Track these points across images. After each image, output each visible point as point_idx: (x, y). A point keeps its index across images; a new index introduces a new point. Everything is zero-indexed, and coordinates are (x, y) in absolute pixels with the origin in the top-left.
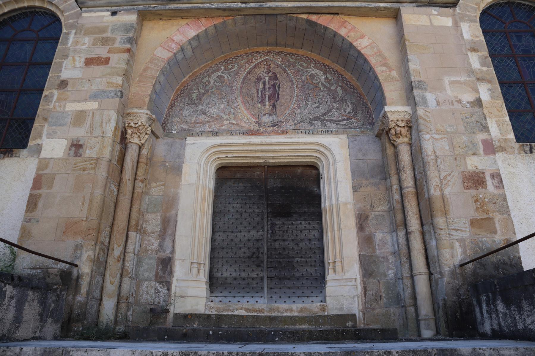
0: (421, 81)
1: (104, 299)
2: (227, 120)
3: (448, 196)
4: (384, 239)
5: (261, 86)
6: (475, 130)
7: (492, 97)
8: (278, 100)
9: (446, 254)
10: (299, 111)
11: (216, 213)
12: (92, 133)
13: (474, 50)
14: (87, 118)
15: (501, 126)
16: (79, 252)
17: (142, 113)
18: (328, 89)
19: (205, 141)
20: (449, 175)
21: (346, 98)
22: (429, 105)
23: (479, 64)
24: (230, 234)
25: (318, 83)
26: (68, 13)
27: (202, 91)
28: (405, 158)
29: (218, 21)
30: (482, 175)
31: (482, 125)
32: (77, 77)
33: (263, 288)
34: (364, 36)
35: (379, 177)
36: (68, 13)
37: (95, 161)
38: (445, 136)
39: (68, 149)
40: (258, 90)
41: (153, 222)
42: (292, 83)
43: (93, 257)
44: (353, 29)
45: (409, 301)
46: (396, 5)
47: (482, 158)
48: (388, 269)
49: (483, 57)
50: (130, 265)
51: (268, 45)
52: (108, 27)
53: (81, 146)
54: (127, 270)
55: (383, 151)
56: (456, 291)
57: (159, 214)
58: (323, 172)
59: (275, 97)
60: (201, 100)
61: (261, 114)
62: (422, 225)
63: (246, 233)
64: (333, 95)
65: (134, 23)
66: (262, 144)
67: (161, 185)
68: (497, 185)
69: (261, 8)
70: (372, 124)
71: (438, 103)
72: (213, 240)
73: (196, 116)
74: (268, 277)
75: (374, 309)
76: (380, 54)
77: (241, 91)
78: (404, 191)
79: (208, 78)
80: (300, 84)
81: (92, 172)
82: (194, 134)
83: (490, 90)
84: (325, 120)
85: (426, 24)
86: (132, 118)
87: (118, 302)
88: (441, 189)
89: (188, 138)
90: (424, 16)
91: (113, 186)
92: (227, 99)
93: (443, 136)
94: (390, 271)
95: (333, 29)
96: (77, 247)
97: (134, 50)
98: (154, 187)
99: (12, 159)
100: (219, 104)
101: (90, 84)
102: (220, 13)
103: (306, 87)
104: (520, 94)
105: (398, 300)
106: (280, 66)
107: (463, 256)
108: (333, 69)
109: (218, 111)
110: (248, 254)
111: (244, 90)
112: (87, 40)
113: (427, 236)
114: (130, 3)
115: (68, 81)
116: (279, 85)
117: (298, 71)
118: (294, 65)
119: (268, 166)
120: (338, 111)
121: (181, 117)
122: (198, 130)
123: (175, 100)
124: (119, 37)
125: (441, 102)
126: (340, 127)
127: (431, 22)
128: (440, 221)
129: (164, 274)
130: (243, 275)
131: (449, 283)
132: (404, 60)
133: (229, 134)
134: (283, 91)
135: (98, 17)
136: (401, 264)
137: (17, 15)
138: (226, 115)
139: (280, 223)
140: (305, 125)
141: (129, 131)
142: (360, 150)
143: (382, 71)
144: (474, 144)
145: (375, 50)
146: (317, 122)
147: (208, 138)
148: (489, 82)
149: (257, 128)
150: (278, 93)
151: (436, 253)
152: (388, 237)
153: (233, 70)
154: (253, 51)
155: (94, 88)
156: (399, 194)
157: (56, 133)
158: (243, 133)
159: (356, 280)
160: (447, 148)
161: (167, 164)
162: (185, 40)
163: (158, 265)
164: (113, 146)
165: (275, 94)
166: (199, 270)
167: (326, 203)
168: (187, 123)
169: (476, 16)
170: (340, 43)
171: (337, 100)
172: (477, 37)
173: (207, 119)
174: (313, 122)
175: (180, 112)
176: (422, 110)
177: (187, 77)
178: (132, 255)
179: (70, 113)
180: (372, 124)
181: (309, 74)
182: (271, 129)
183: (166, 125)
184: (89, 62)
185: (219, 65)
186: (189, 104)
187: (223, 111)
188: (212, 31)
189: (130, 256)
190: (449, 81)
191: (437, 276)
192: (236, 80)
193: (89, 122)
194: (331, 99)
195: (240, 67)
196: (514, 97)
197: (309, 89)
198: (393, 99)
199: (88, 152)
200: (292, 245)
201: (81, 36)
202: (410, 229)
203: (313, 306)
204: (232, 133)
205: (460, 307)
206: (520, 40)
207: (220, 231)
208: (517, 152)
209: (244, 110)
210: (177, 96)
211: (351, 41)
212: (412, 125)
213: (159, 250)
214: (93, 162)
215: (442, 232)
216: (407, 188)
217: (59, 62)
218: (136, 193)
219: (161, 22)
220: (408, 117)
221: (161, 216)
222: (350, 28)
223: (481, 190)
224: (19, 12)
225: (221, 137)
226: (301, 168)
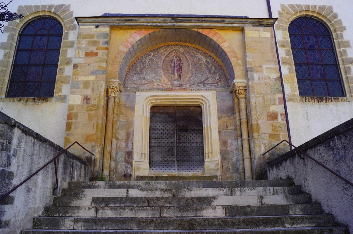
0: (252, 68)
1: (104, 170)
2: (156, 83)
3: (260, 124)
4: (232, 143)
5: (173, 65)
6: (275, 93)
7: (289, 73)
8: (182, 72)
9: (257, 149)
10: (192, 78)
11: (151, 129)
12: (93, 92)
13: (283, 46)
15: (292, 88)
16: (94, 149)
17: (116, 81)
18: (207, 67)
20: (261, 114)
21: (216, 71)
22: (255, 80)
23: (285, 54)
24: (158, 140)
25: (202, 63)
26: (66, 21)
27: (142, 67)
28: (243, 105)
29: (151, 31)
30: (276, 114)
31: (279, 90)
32: (81, 62)
33: (174, 165)
34: (226, 41)
35: (231, 113)
36: (66, 21)
37: (96, 106)
38: (261, 95)
39: (83, 100)
41: (122, 134)
45: (241, 171)
46: (242, 25)
47: (277, 106)
48: (233, 156)
49: (288, 50)
50: (114, 155)
51: (176, 41)
52: (94, 34)
54: (112, 157)
55: (233, 100)
56: (260, 166)
57: (125, 131)
58: (204, 110)
59: (180, 70)
60: (142, 72)
61: (173, 80)
62: (249, 137)
63: (166, 140)
64: (209, 70)
65: (108, 32)
66: (174, 96)
68: (283, 119)
69: (173, 26)
70: (229, 86)
71: (259, 79)
72: (150, 143)
73: (140, 80)
74: (177, 160)
75: (226, 174)
76: (234, 52)
77: (163, 67)
78: (241, 120)
81: (96, 112)
83: (289, 69)
84: (205, 83)
85: (257, 36)
86: (111, 84)
87: (110, 172)
88: (257, 121)
89: (137, 92)
90: (256, 31)
92: (155, 71)
93: (260, 95)
94: (234, 158)
95: (210, 37)
96: (93, 147)
97: (109, 48)
98: (121, 117)
99: (47, 103)
101: (89, 66)
102: (153, 27)
103: (196, 65)
104: (305, 70)
105: (237, 170)
106: (182, 53)
107: (264, 151)
108: (210, 55)
109: (151, 78)
110: (167, 150)
111: (164, 67)
112: (84, 42)
113: (250, 142)
114: (105, 21)
115: (77, 65)
116: (182, 64)
117: (192, 56)
118: (189, 53)
119: (177, 106)
121: (132, 81)
122: (142, 88)
123: (128, 71)
124: (101, 40)
125: (261, 78)
126: (212, 87)
127: (259, 35)
128: (255, 134)
129: (129, 159)
130: (166, 159)
131: (257, 162)
132: (245, 56)
134: (184, 67)
135: (88, 28)
136: (239, 154)
137: (35, 20)
138: (155, 80)
139: (183, 134)
140: (195, 86)
141: (110, 90)
142: (222, 99)
143: (234, 61)
144: (274, 100)
145: (231, 49)
147: (147, 92)
148: (289, 64)
149: (171, 87)
151: (253, 149)
152: (234, 142)
154: (168, 44)
155: (92, 69)
156: (239, 122)
157: (75, 92)
158: (164, 90)
159: (218, 161)
160: (261, 101)
161: (127, 106)
162: (134, 42)
163: (126, 155)
164: (104, 99)
165: (180, 69)
166: (145, 157)
167: (205, 125)
169: (286, 27)
170: (214, 44)
171: (211, 73)
172: (286, 39)
173: (146, 82)
175: (132, 78)
176: (251, 82)
177: (134, 58)
178: (114, 150)
179: (81, 82)
180: (229, 86)
182: (178, 88)
183: (125, 85)
184: (87, 54)
185: (150, 52)
186: (136, 74)
187: (154, 78)
188: (148, 36)
189: (113, 151)
190: (266, 67)
191: (253, 159)
195: (162, 53)
196: (302, 72)
197: (198, 66)
198: (238, 75)
199: (93, 101)
200: (189, 145)
201: (81, 39)
202: (243, 138)
203: (199, 173)
204: (159, 90)
205: (262, 172)
206: (309, 40)
207: (153, 138)
208: (298, 101)
209: (164, 78)
210: (129, 69)
211: (219, 44)
212: (246, 89)
213: (126, 148)
214: (96, 107)
215: (256, 140)
216: (243, 119)
217: (65, 50)
219: (121, 31)
220: (245, 85)
221: (126, 131)
223: (275, 121)
224: (37, 18)
225: (154, 92)
226: (193, 107)
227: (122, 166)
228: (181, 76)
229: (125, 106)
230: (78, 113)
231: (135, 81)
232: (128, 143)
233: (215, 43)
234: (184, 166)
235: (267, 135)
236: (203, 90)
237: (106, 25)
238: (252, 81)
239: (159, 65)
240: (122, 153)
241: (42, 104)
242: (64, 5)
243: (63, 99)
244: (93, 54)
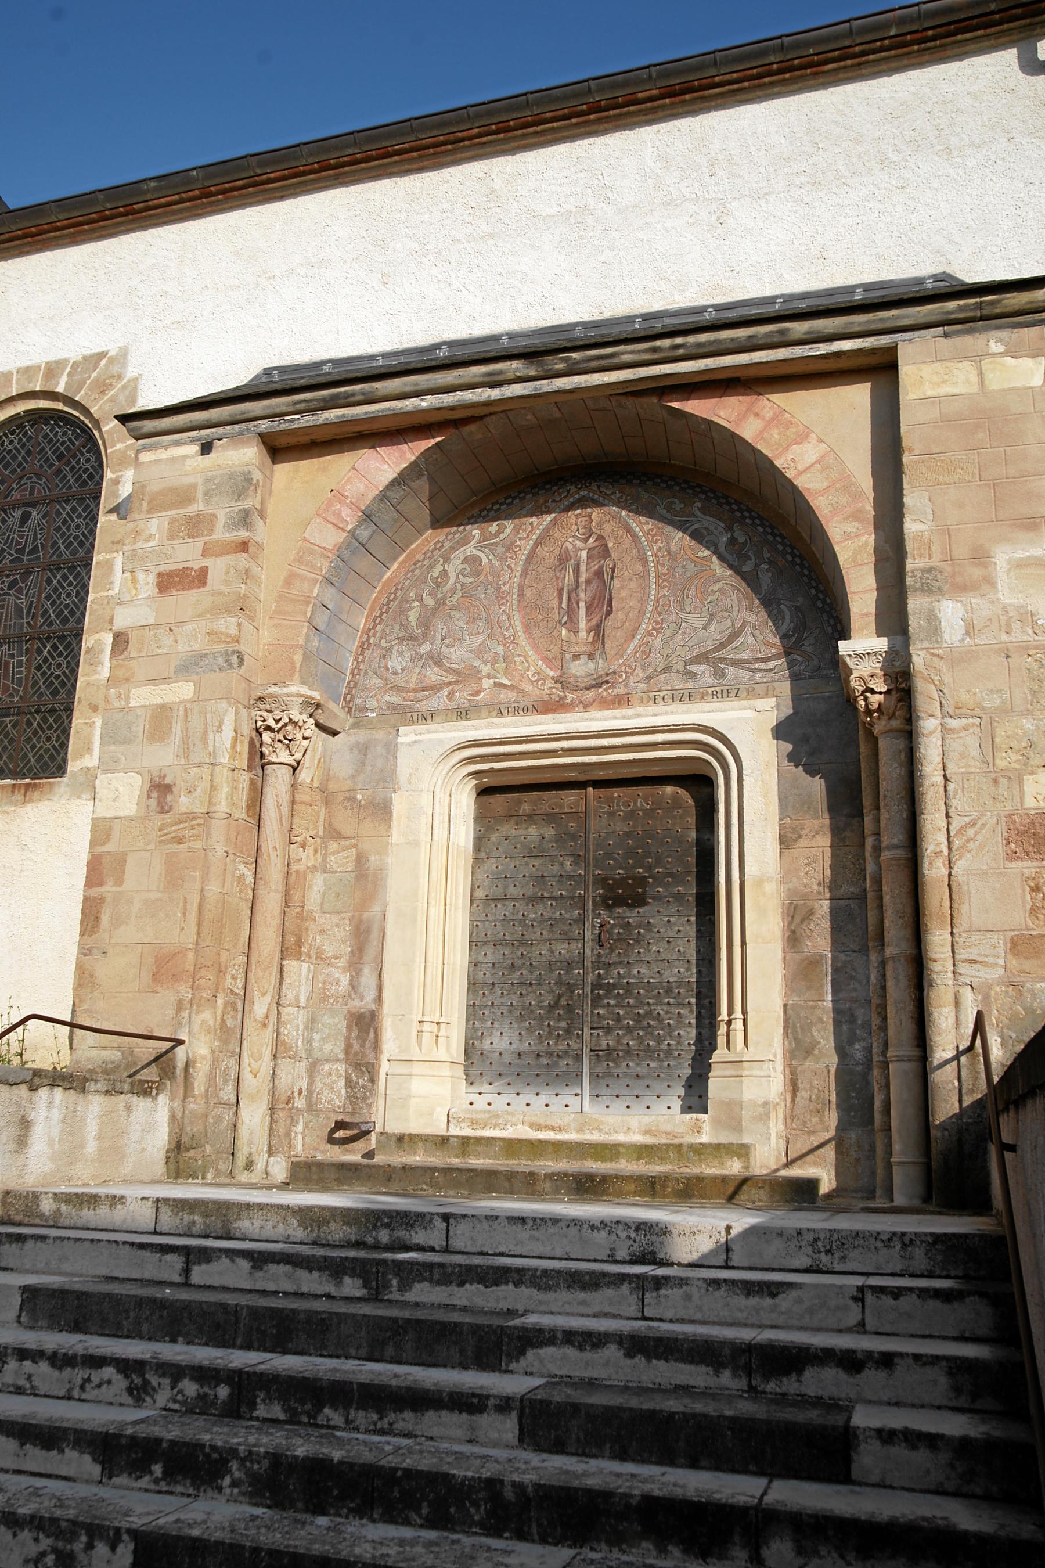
0: (930, 570)
2: (489, 677)
5: (569, 577)
8: (609, 613)
10: (659, 640)
12: (187, 757)
14: (174, 723)
19: (441, 735)
20: (972, 824)
22: (946, 636)
27: (430, 602)
42: (644, 561)
43: (211, 1023)
44: (778, 418)
52: (194, 486)
54: (284, 1043)
59: (603, 604)
61: (568, 656)
67: (348, 848)
77: (521, 595)
80: (663, 565)
82: (415, 718)
84: (722, 660)
89: (402, 729)
91: (242, 867)
92: (488, 620)
94: (857, 1046)
98: (333, 854)
100: (470, 634)
103: (679, 570)
108: (750, 511)
111: (528, 593)
116: (613, 571)
120: (757, 633)
124: (223, 511)
129: (363, 1046)
133: (495, 713)
134: (622, 587)
135: (173, 460)
138: (485, 662)
143: (847, 537)
146: (703, 667)
150: (610, 595)
153: (502, 536)
155: (181, 647)
158: (525, 710)
163: (349, 1028)
168: (396, 688)
174: (694, 668)
182: (589, 695)
183: (353, 697)
184: (167, 582)
186: (401, 640)
187: (479, 653)
190: (1009, 561)
192: (509, 567)
193: (179, 732)
194: (739, 602)
199: (183, 799)
201: (142, 516)
210: (374, 620)
217: (107, 561)
218: (294, 874)
222: (768, 415)
227: (334, 1082)
229: (349, 799)
230: (125, 854)
231: (396, 673)
232: (359, 973)
234: (624, 1082)
235: (1000, 941)
236: (709, 698)
237: (241, 433)
238: (926, 645)
239: (503, 588)
240: (337, 1020)
241: (21, 811)
242: (102, 355)
243: (89, 786)
244: (188, 576)
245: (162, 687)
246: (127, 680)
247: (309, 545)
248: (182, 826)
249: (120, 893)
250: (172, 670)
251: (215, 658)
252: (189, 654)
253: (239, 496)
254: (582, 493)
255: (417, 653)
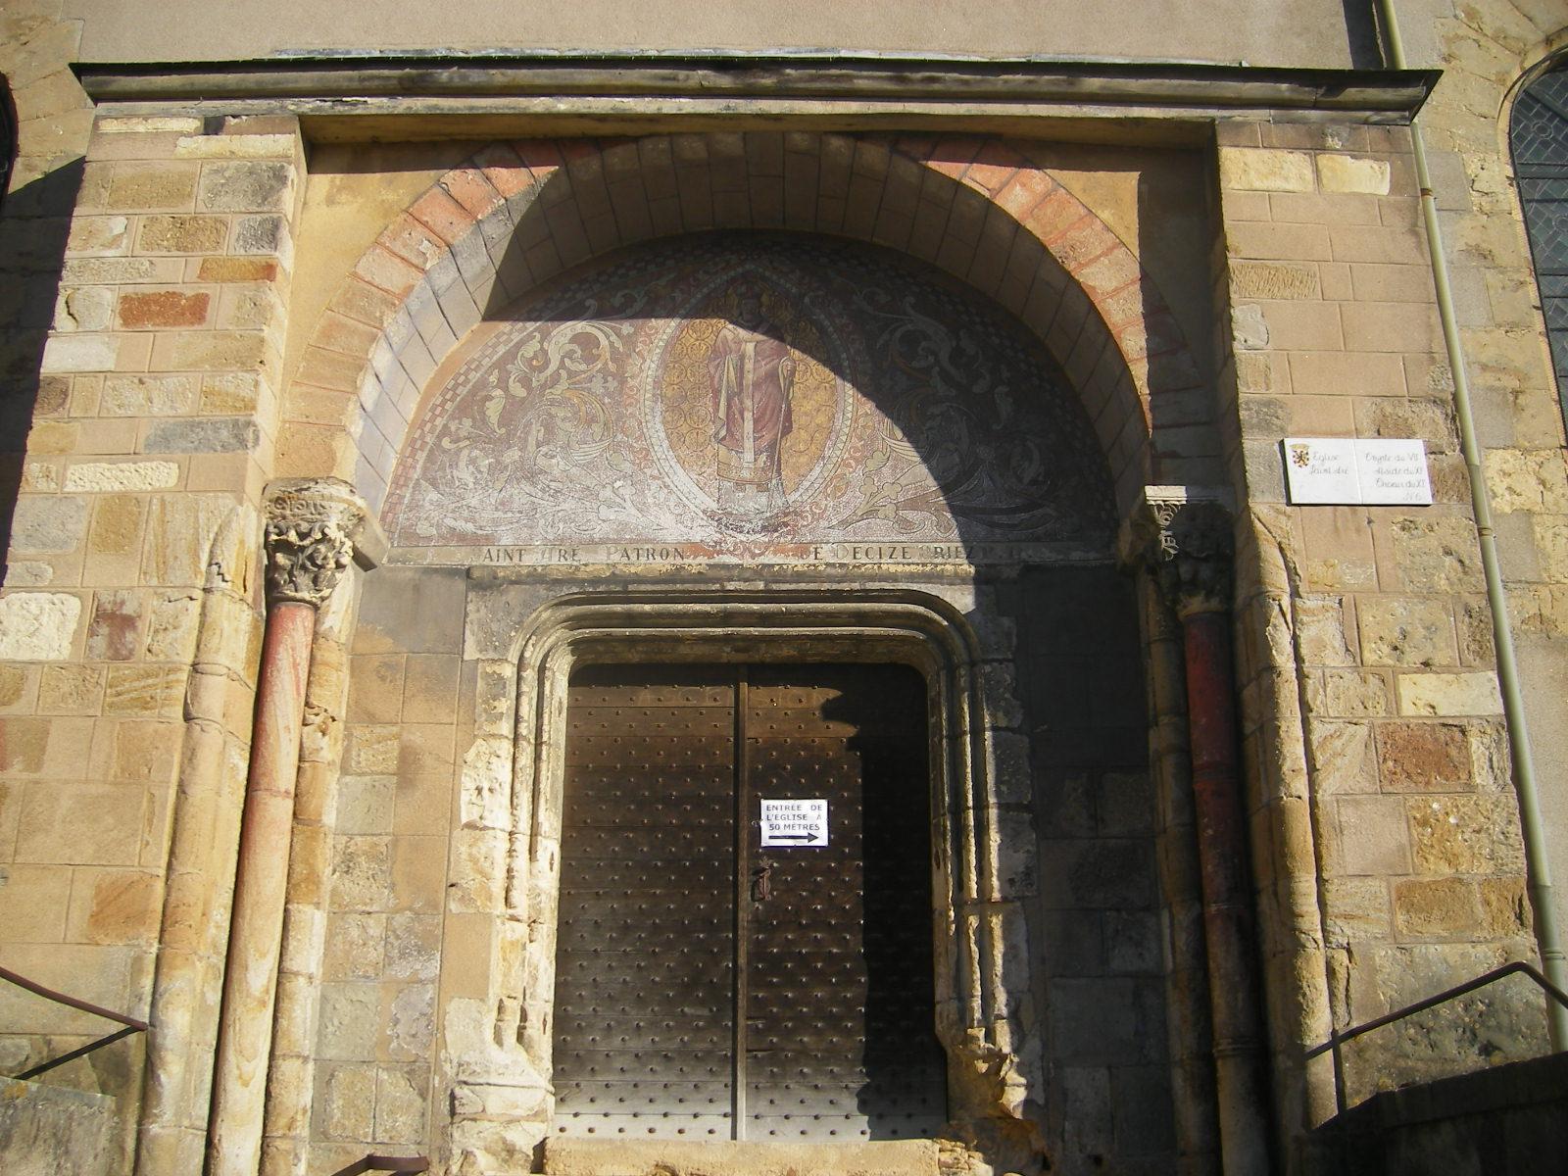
0: (1269, 403)
8: (787, 430)
12: (162, 577)
27: (521, 392)
40: (716, 393)
53: (127, 622)
79: (541, 342)
135: (156, 135)
181: (898, 334)
201: (101, 210)
210: (433, 410)
228: (784, 457)
233: (1017, 227)
239: (631, 382)
244: (173, 305)
245: (123, 466)
246: (62, 450)
247: (362, 284)
248: (150, 681)
249: (37, 782)
250: (142, 441)
251: (216, 430)
252: (171, 421)
253: (265, 199)
254: (747, 267)
255: (498, 462)
